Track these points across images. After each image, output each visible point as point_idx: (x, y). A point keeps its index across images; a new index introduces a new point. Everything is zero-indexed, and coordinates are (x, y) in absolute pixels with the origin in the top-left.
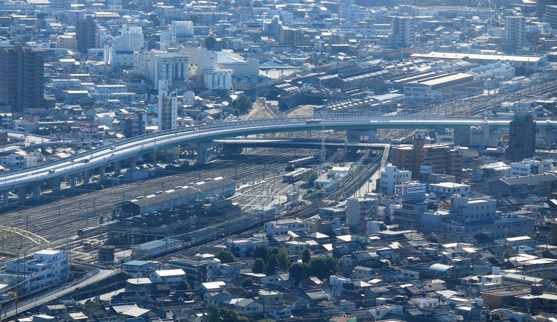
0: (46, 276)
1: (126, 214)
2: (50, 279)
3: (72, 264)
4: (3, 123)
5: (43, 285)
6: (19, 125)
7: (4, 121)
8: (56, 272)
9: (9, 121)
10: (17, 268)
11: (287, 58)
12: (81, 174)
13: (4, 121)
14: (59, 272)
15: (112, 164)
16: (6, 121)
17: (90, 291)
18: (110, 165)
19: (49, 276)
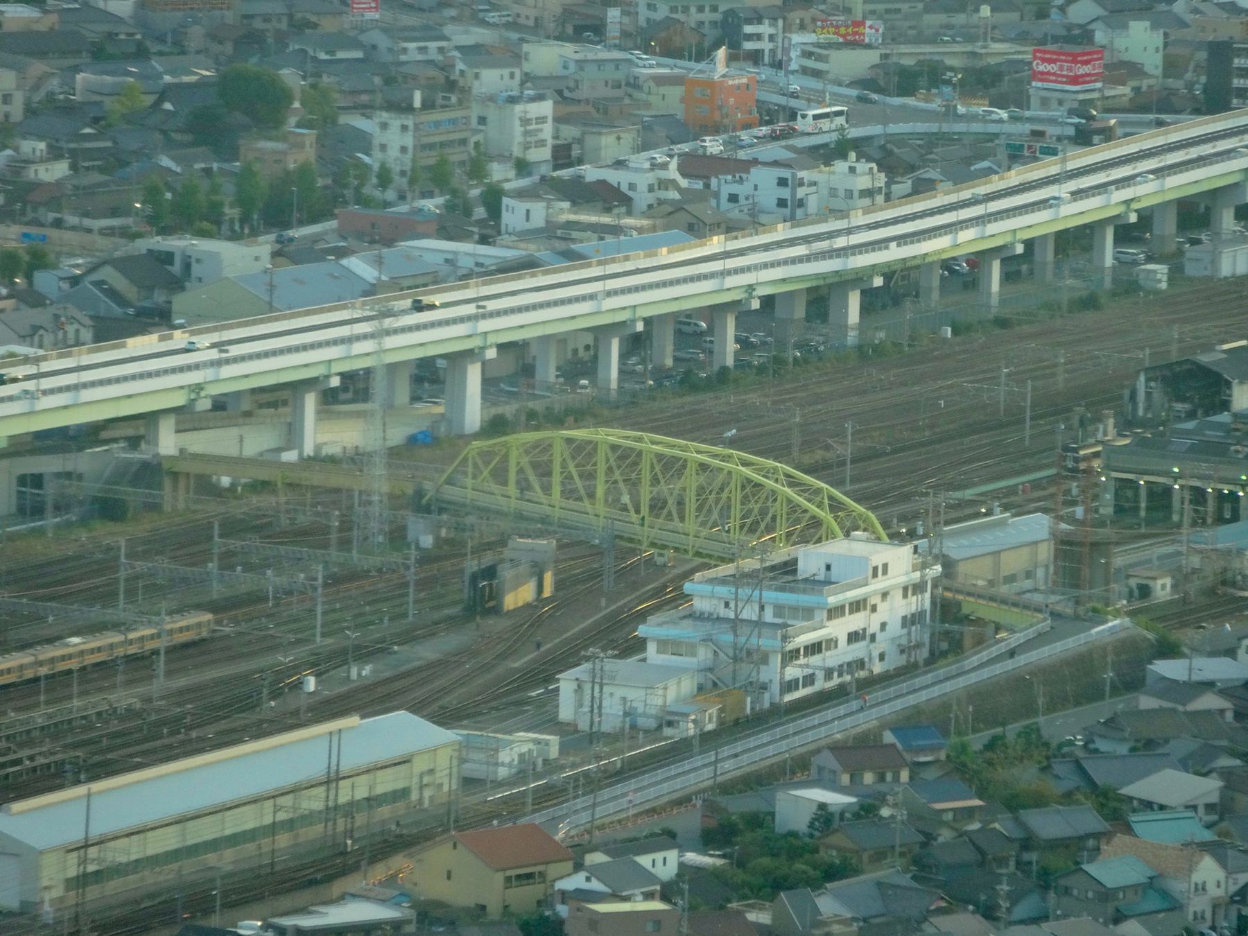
0: (843, 640)
1: (1179, 406)
2: (858, 650)
3: (949, 595)
4: (749, 46)
5: (829, 673)
6: (807, 55)
7: (749, 37)
8: (883, 626)
9: (772, 38)
10: (732, 605)
11: (1041, 48)
12: (1020, 249)
13: (749, 37)
14: (895, 628)
15: (648, 321)
16: (759, 37)
17: (424, 674)
18: (640, 327)
19: (854, 637)
